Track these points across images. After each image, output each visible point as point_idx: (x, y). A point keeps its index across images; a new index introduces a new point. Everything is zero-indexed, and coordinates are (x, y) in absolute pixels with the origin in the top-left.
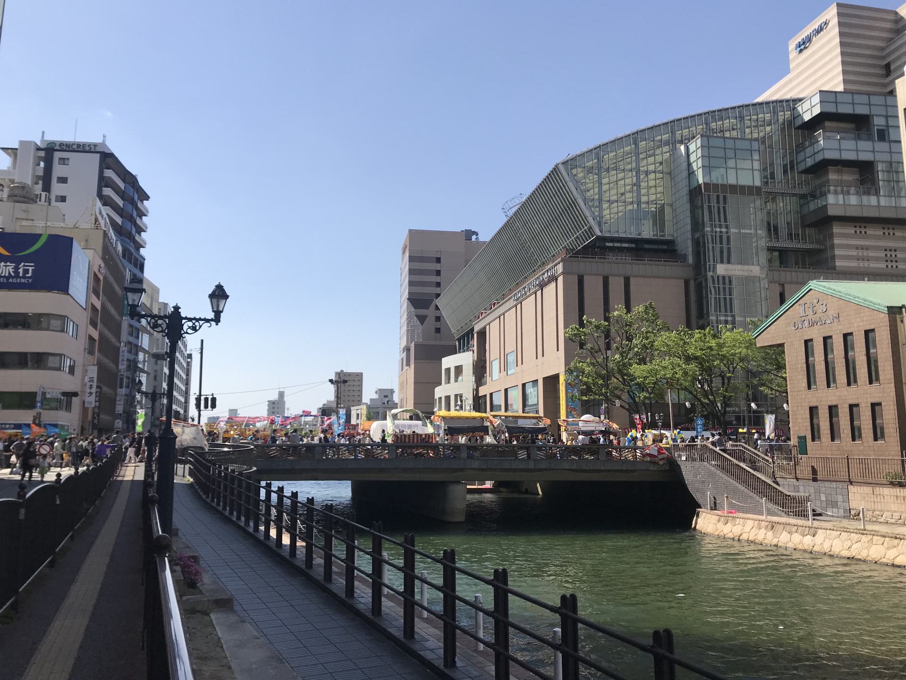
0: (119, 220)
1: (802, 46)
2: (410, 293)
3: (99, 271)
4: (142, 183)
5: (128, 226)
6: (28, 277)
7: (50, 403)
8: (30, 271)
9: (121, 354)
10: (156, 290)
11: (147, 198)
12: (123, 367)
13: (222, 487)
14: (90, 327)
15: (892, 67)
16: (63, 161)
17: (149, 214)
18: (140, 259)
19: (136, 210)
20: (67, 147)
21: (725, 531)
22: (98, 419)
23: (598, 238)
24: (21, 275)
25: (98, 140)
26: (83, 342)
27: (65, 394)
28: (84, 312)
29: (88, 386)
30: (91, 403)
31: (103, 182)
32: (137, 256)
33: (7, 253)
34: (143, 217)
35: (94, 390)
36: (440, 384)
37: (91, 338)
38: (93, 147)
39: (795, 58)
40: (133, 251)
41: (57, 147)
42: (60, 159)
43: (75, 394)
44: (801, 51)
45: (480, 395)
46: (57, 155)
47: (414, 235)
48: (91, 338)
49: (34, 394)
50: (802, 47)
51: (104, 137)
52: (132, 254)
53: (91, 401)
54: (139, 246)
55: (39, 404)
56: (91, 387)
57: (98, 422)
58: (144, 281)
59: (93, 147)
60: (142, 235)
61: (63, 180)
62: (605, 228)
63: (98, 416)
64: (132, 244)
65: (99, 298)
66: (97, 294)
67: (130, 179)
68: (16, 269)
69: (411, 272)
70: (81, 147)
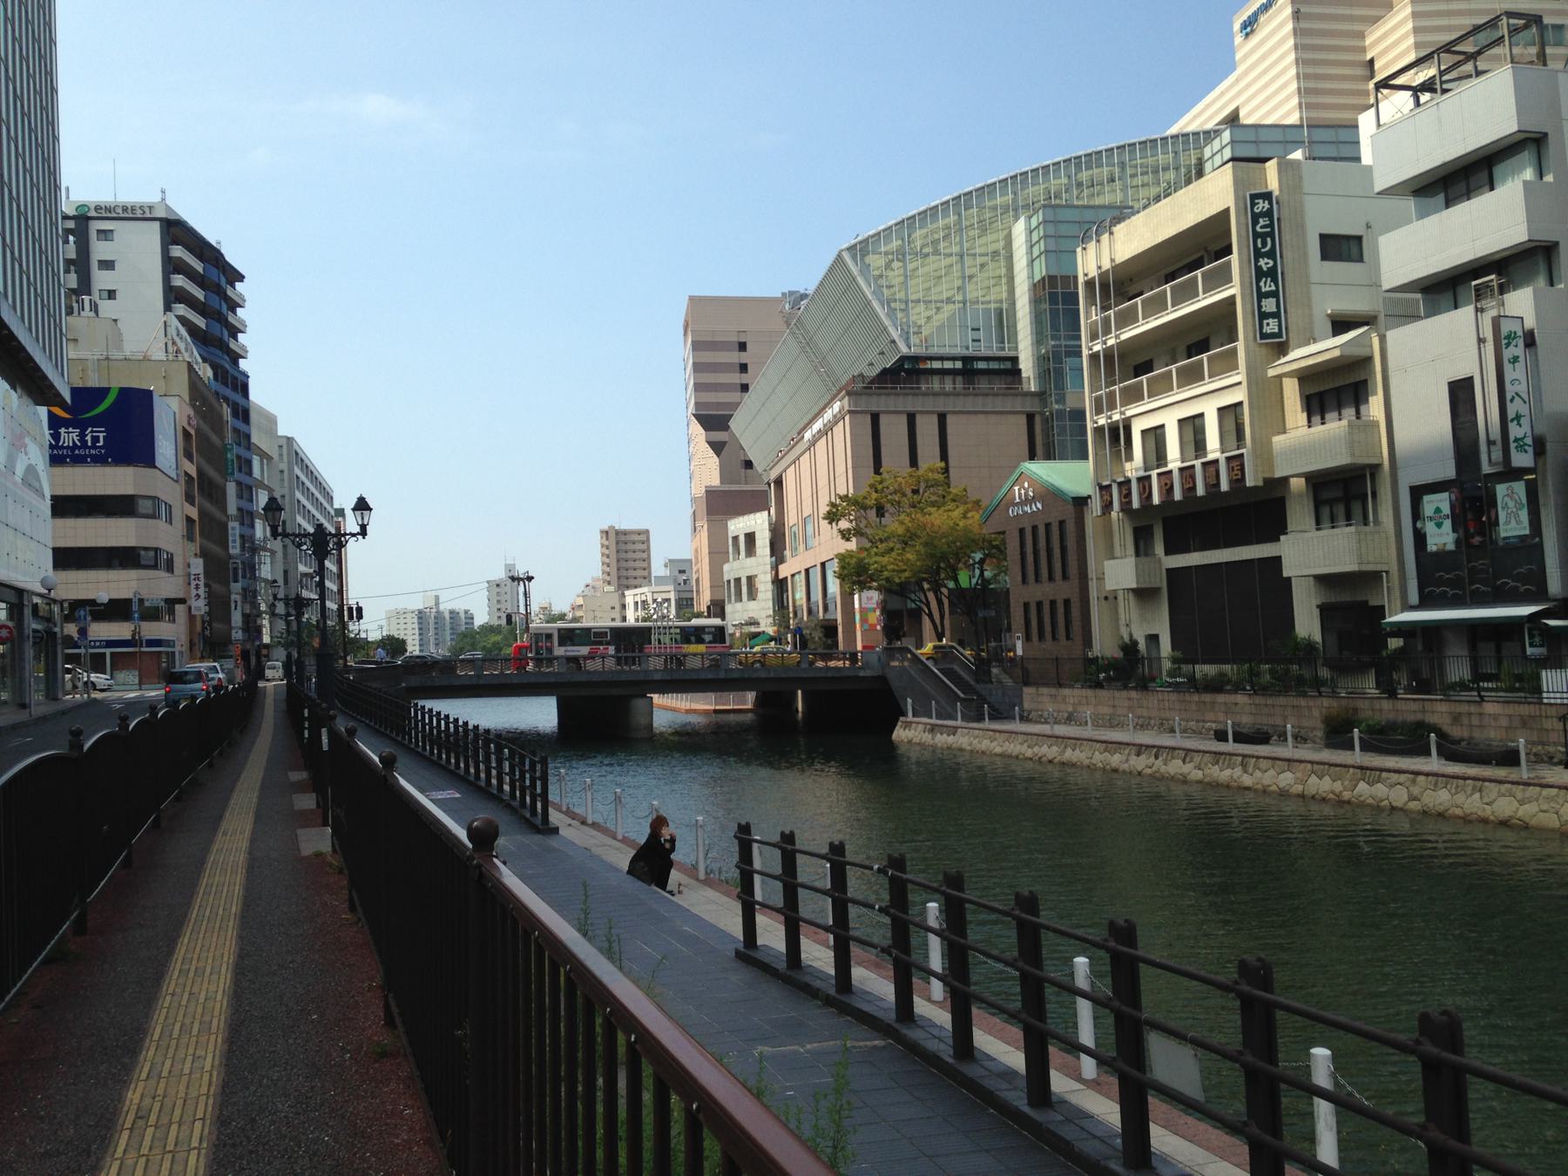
0: (201, 322)
1: (1250, 26)
2: (697, 404)
3: (189, 424)
4: (232, 257)
5: (217, 329)
6: (100, 447)
7: (152, 614)
8: (101, 439)
9: (230, 531)
10: (272, 420)
11: (241, 278)
12: (235, 549)
13: (527, 763)
14: (187, 505)
15: (1377, 66)
16: (105, 235)
17: (247, 304)
18: (241, 377)
19: (225, 302)
20: (110, 213)
21: (1266, 782)
22: (211, 629)
23: (903, 359)
24: (89, 444)
25: (151, 197)
26: (179, 525)
27: (167, 601)
28: (176, 485)
29: (193, 586)
30: (198, 609)
31: (171, 266)
32: (236, 374)
33: (67, 416)
34: (239, 334)
35: (202, 591)
36: (728, 561)
37: (189, 520)
38: (147, 210)
39: (1241, 45)
40: (227, 366)
41: (93, 214)
42: (99, 231)
43: (182, 601)
44: (1247, 35)
45: (781, 577)
46: (95, 226)
47: (698, 304)
48: (189, 520)
49: (128, 602)
50: (1249, 29)
51: (163, 192)
52: (227, 372)
53: (200, 606)
54: (235, 357)
55: (136, 615)
56: (197, 587)
57: (211, 633)
58: (253, 416)
59: (147, 210)
60: (239, 340)
61: (108, 265)
62: (914, 340)
63: (210, 625)
64: (226, 357)
65: (192, 461)
66: (189, 456)
67: (209, 253)
68: (82, 436)
69: (698, 367)
70: (129, 211)
